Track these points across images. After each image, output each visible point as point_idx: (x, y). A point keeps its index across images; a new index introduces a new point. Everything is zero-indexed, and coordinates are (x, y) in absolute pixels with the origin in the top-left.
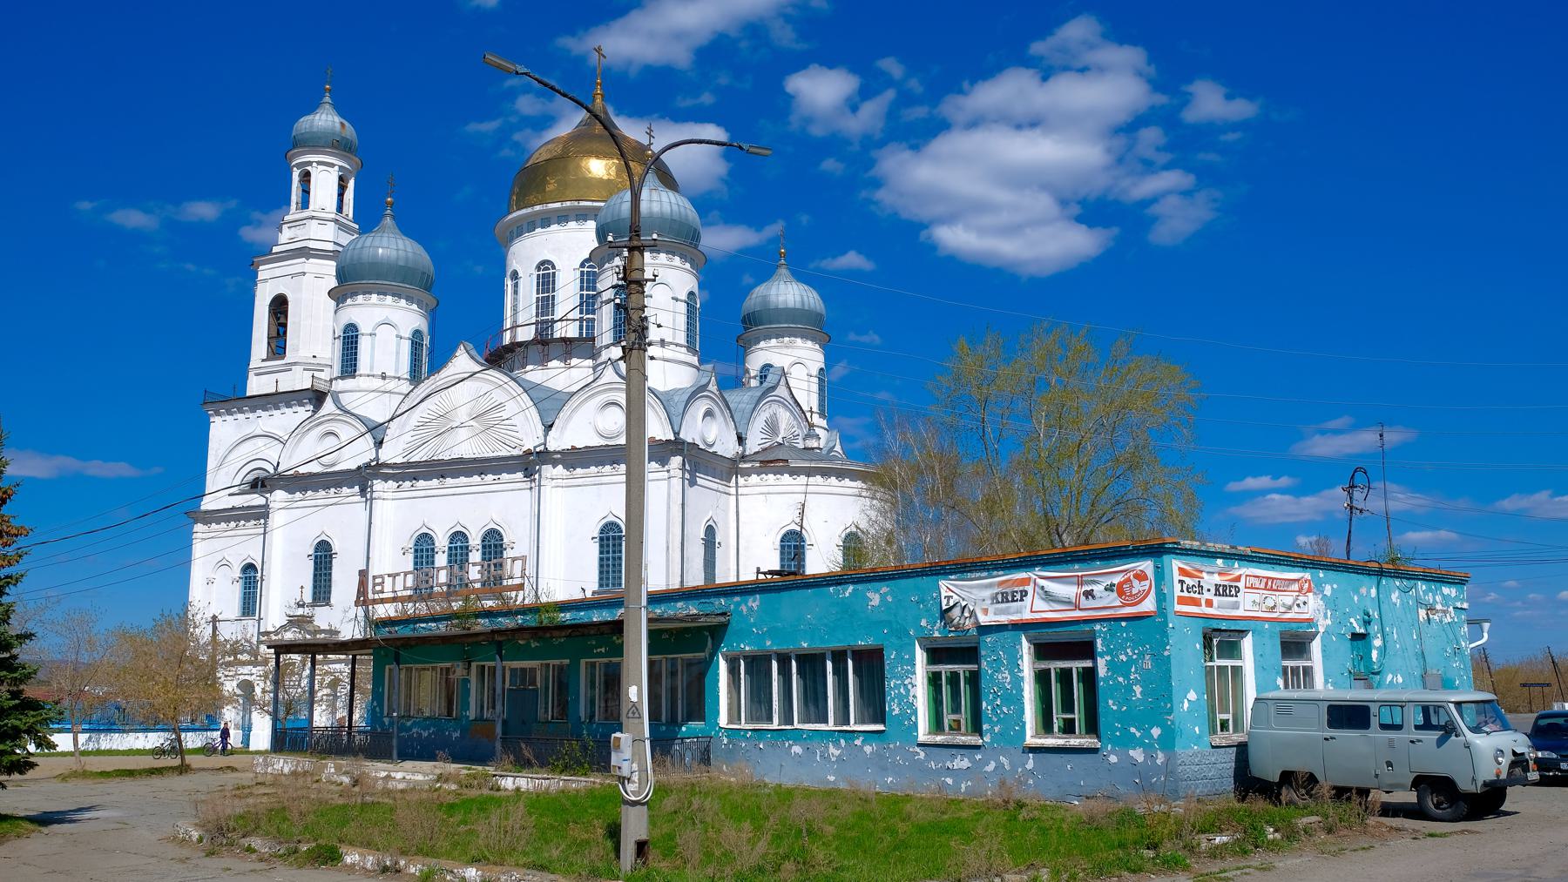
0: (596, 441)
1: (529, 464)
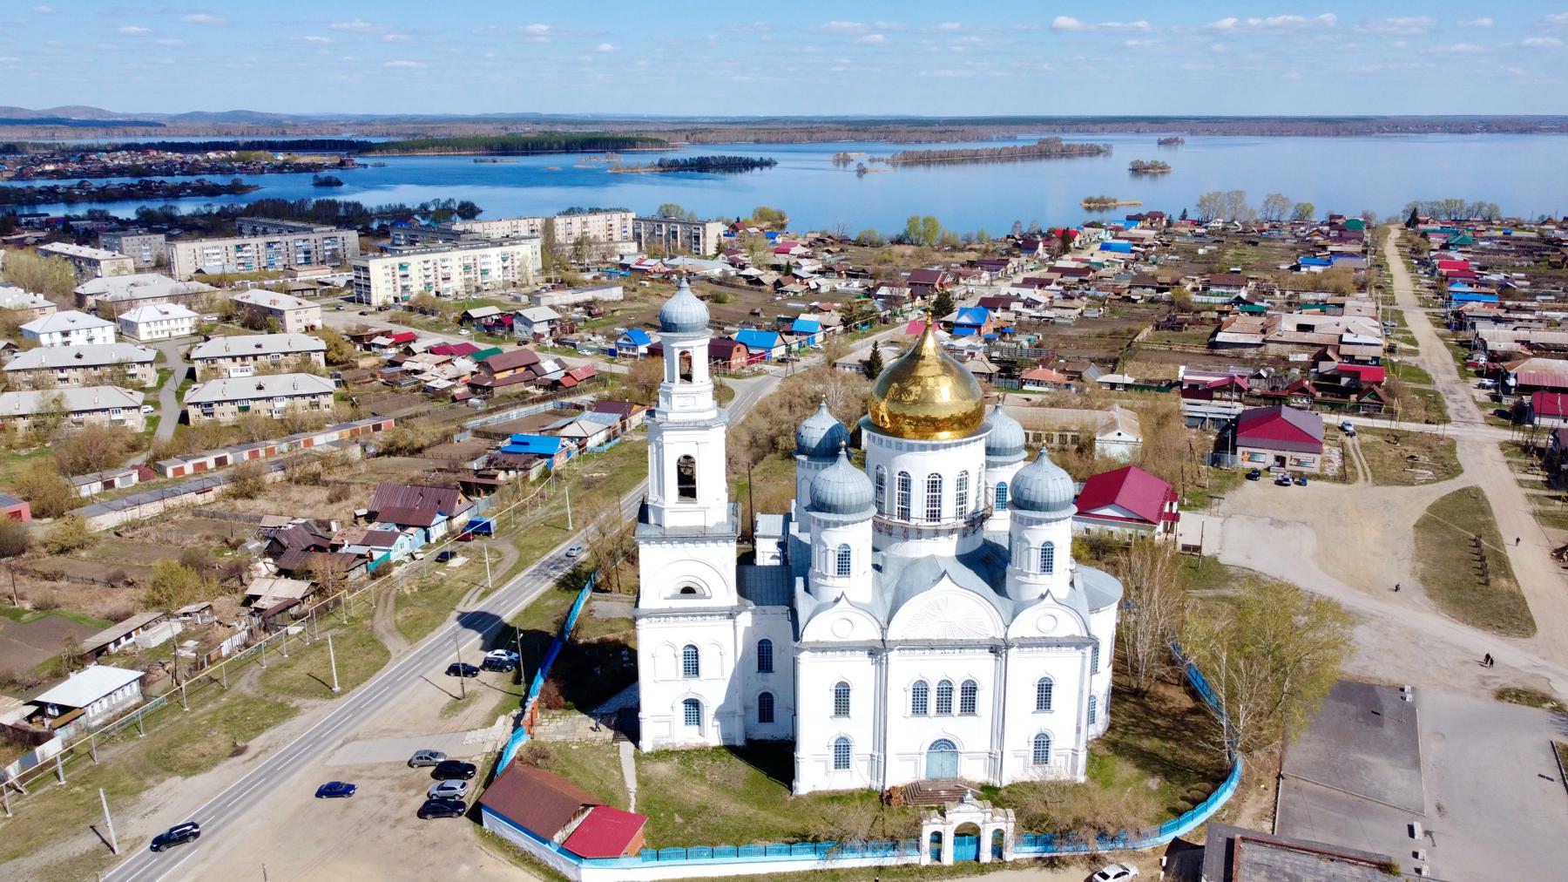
0: (1037, 634)
1: (997, 649)
